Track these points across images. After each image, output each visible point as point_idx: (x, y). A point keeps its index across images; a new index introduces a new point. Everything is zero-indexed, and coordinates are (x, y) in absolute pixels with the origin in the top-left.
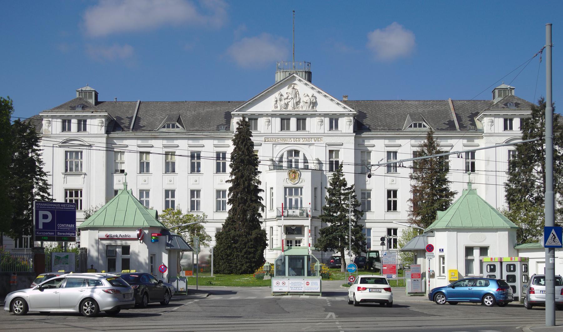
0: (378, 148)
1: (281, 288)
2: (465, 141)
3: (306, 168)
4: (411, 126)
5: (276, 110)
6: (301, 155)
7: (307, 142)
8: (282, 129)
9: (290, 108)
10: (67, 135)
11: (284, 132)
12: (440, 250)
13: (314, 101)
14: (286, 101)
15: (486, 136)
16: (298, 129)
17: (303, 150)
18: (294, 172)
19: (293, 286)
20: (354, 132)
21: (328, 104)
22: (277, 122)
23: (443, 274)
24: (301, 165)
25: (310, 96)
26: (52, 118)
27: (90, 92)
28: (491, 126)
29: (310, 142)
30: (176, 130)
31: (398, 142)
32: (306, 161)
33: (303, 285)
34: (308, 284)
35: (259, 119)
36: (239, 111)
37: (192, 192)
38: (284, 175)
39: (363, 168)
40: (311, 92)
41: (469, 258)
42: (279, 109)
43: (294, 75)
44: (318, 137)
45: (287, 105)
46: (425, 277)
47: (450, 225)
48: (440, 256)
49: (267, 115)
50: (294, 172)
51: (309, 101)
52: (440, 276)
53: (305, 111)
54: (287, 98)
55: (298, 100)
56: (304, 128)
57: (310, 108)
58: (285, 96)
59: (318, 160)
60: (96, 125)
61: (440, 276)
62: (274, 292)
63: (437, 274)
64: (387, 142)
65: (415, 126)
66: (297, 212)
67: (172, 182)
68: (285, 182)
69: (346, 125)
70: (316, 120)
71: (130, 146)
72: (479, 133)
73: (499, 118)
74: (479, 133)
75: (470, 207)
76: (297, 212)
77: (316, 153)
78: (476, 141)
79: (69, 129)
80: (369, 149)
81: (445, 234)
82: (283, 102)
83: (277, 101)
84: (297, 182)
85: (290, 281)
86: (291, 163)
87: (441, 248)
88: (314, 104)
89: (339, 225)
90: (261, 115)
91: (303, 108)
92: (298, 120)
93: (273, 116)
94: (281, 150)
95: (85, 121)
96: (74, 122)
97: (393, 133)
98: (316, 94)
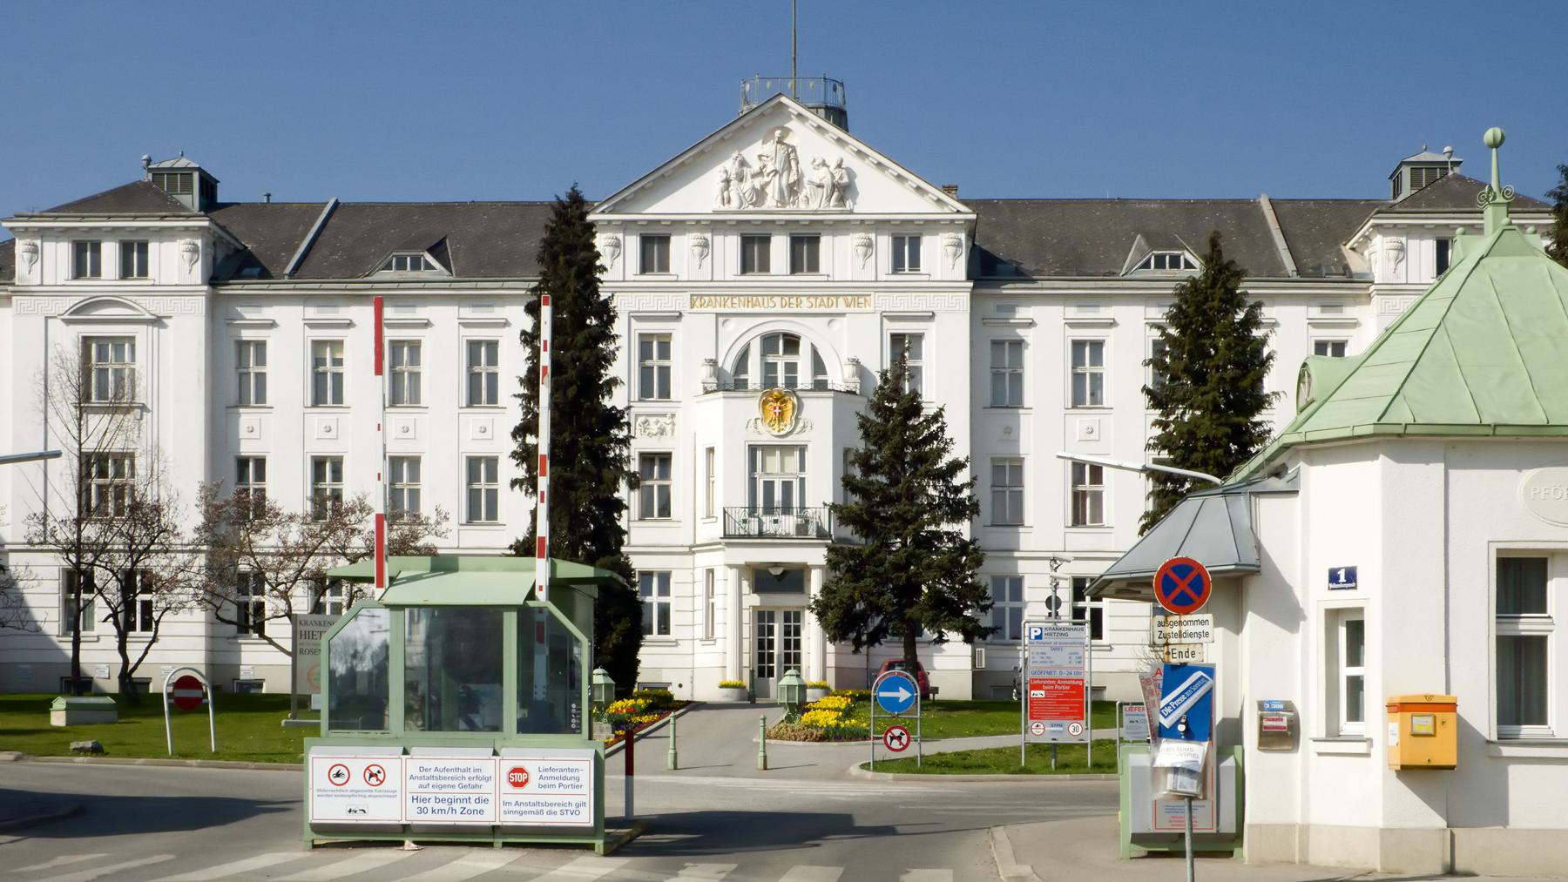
0: (1046, 328)
1: (356, 803)
2: (1315, 312)
3: (820, 386)
4: (1147, 265)
5: (727, 207)
6: (804, 348)
7: (823, 310)
8: (746, 267)
9: (771, 202)
10: (88, 285)
11: (753, 278)
12: (1333, 577)
13: (846, 180)
14: (758, 182)
15: (1380, 292)
16: (795, 267)
17: (810, 333)
18: (781, 399)
19: (430, 792)
20: (969, 278)
21: (887, 192)
22: (729, 247)
23: (1348, 728)
24: (804, 378)
25: (833, 165)
26: (43, 238)
27: (186, 173)
28: (1398, 261)
29: (833, 310)
30: (424, 274)
31: (1106, 313)
32: (818, 365)
33: (487, 787)
34: (518, 779)
35: (673, 239)
36: (611, 212)
37: (473, 464)
38: (749, 406)
39: (999, 382)
40: (833, 154)
41: (1528, 625)
42: (734, 205)
43: (784, 100)
44: (856, 293)
45: (760, 194)
46: (1240, 741)
47: (1402, 415)
48: (1333, 615)
49: (699, 225)
50: (780, 397)
51: (827, 181)
52: (1333, 735)
53: (815, 213)
54: (761, 173)
55: (793, 178)
56: (814, 267)
57: (833, 202)
58: (756, 166)
59: (856, 363)
60: (176, 261)
61: (1333, 735)
62: (320, 829)
63: (1313, 723)
64: (1072, 312)
65: (1160, 263)
66: (788, 524)
67: (410, 434)
68: (752, 428)
69: (944, 258)
70: (854, 240)
71: (285, 329)
72: (1354, 284)
73: (1421, 238)
74: (1354, 284)
75: (1516, 320)
76: (788, 524)
77: (850, 347)
78: (1350, 312)
79: (96, 272)
80: (1021, 332)
81: (1372, 472)
82: (746, 186)
83: (728, 181)
84: (788, 429)
85: (413, 764)
86: (770, 371)
87: (1342, 562)
88: (844, 191)
89: (902, 548)
90: (680, 225)
91: (812, 204)
92: (796, 241)
93: (717, 226)
94: (743, 332)
95: (143, 248)
96: (110, 252)
97: (1092, 284)
98: (852, 161)
